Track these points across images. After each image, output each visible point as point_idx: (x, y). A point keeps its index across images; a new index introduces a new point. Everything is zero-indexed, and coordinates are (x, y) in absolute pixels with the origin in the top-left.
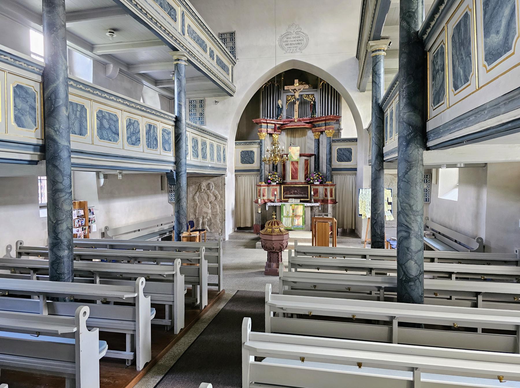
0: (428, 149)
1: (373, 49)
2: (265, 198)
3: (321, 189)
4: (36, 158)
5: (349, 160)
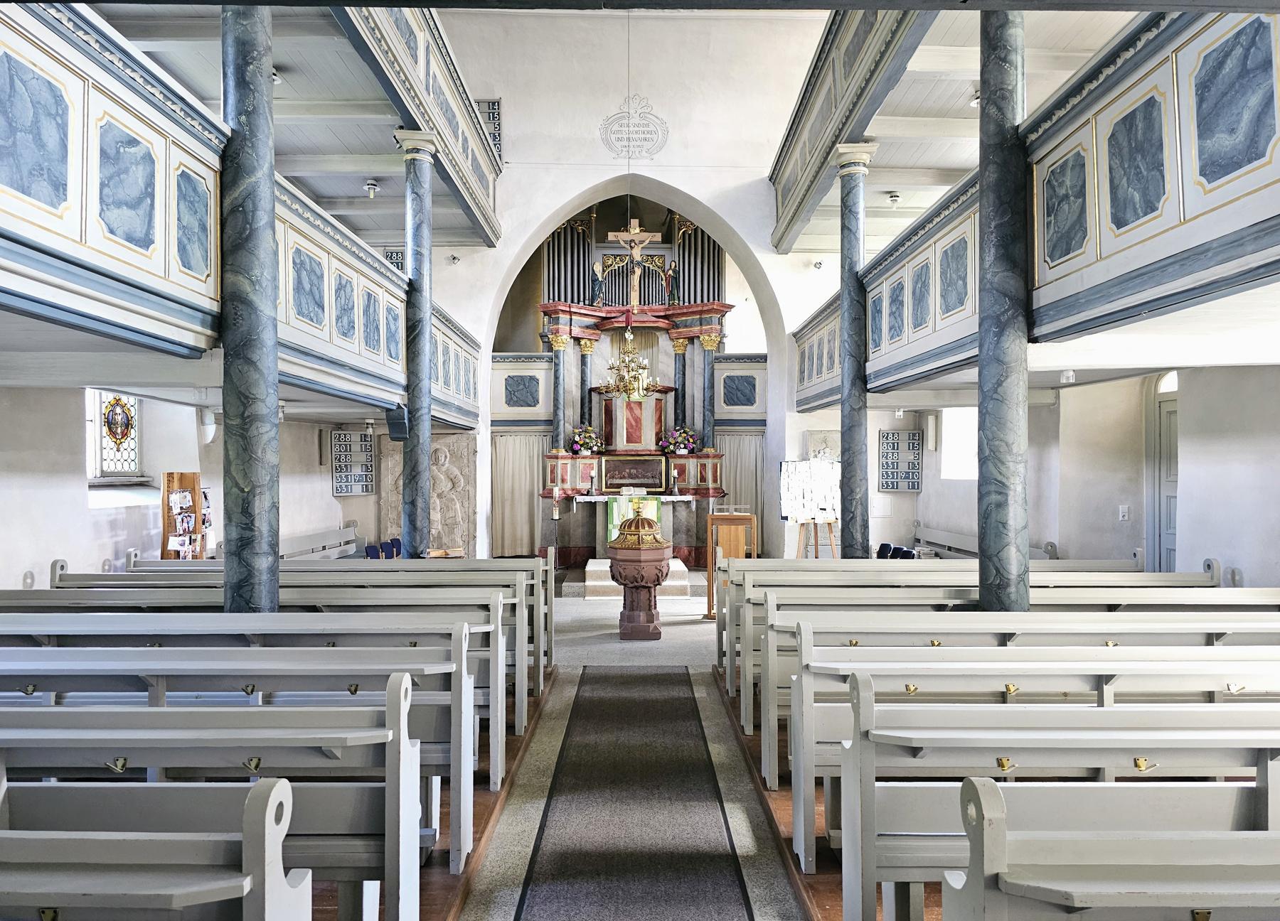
0: (1033, 340)
1: (844, 160)
2: (568, 486)
3: (692, 465)
4: (202, 344)
5: (750, 401)
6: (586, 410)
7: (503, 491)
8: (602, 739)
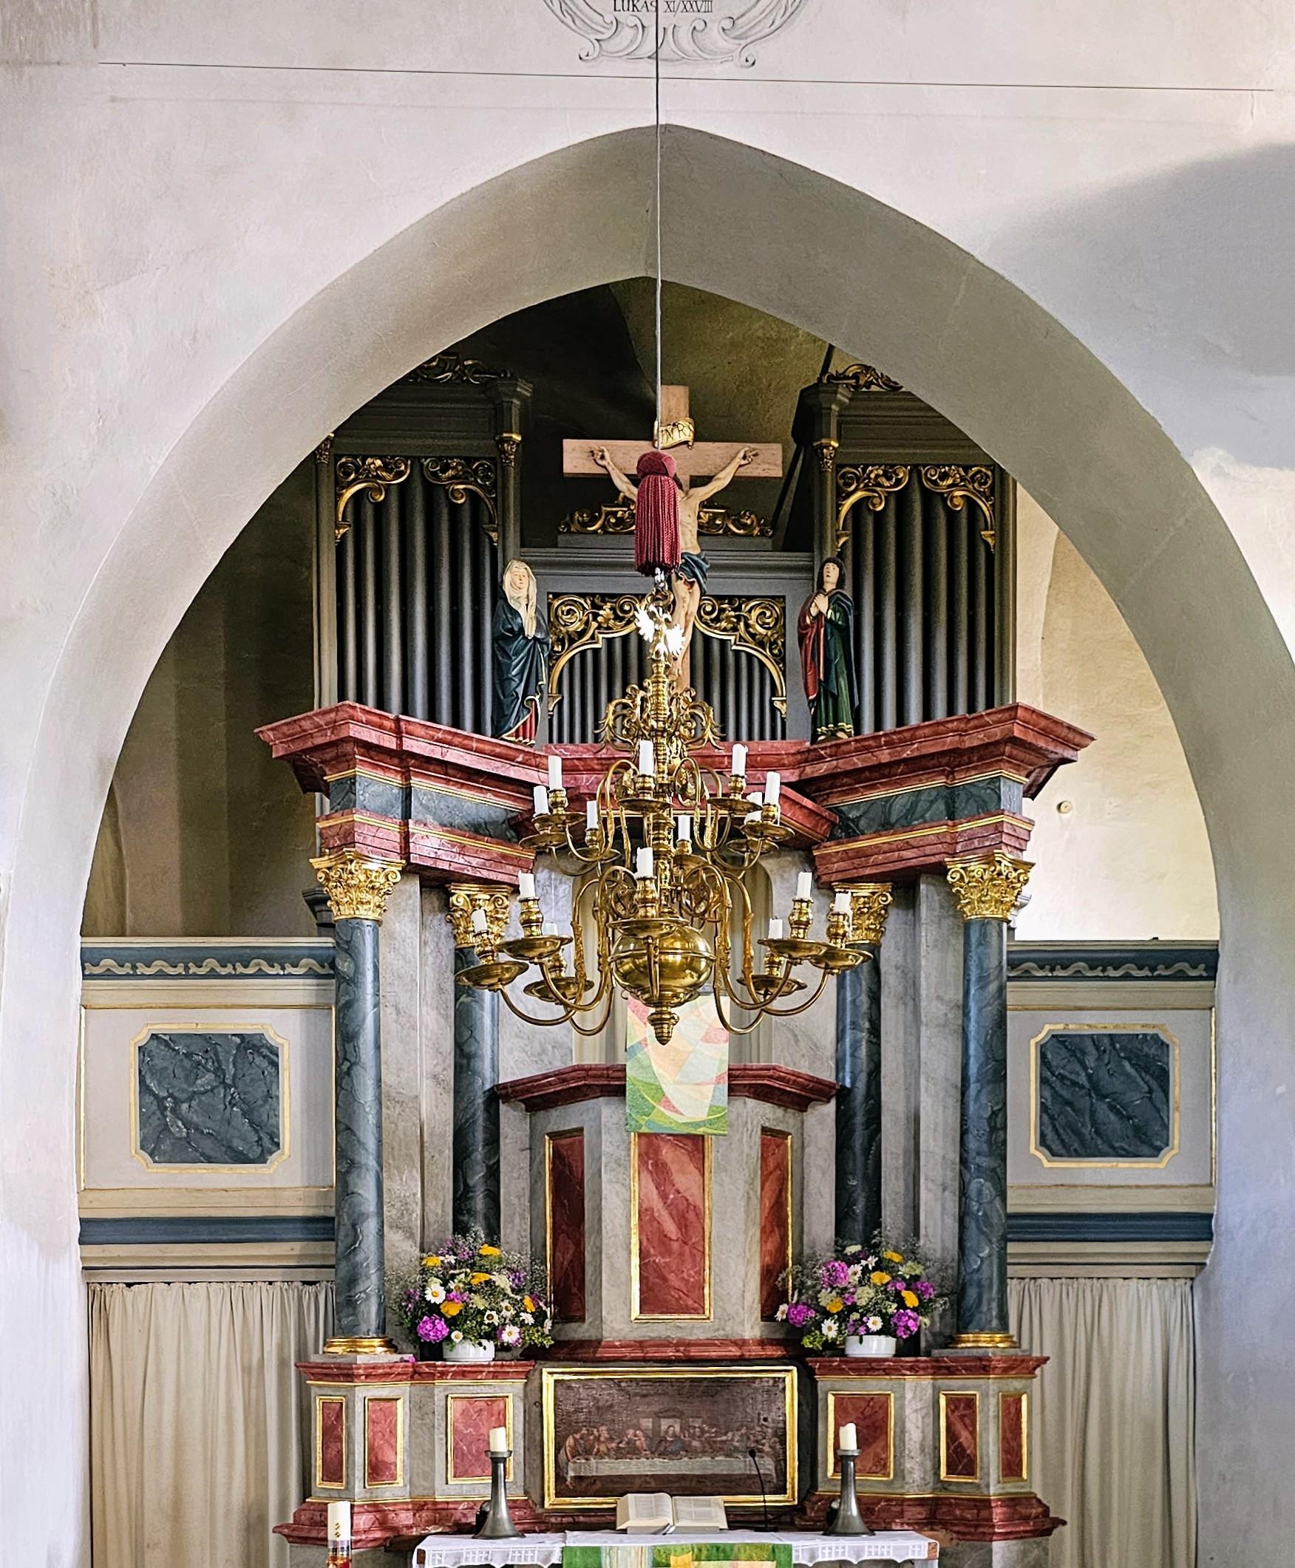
2: (395, 1491)
3: (914, 1403)
5: (1145, 1137)
6: (477, 1177)
7: (137, 1512)
8: (716, 647)
